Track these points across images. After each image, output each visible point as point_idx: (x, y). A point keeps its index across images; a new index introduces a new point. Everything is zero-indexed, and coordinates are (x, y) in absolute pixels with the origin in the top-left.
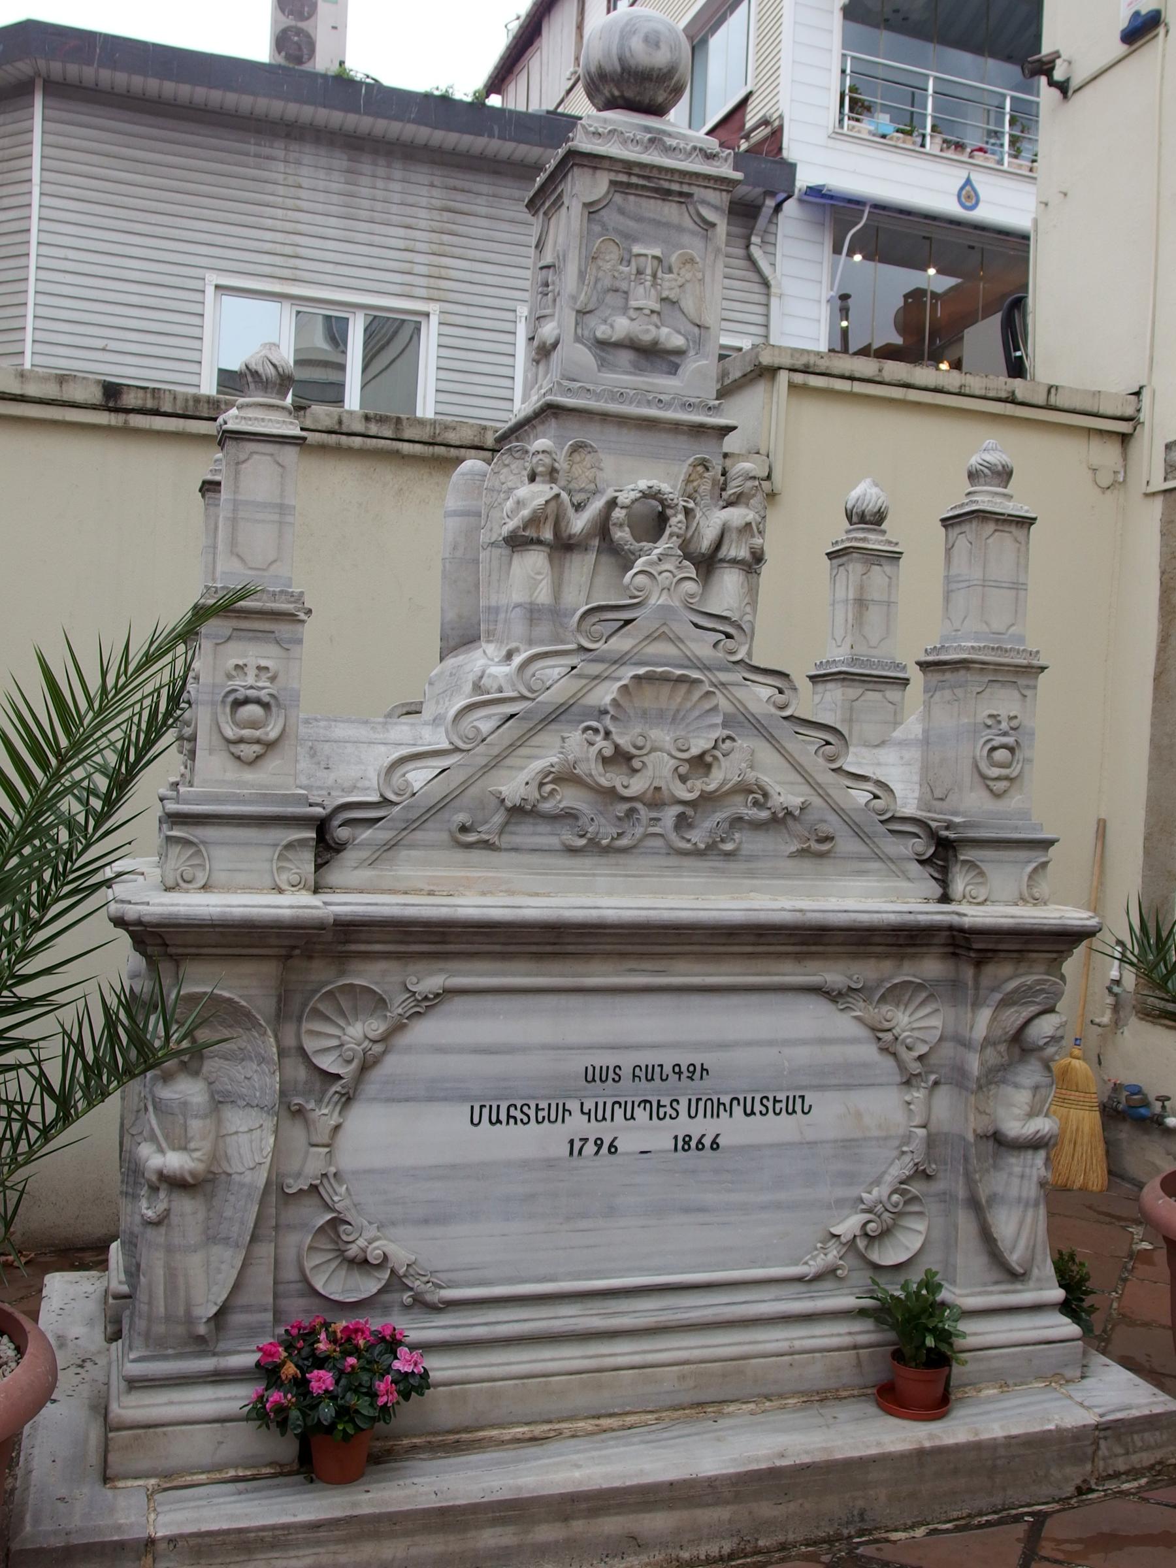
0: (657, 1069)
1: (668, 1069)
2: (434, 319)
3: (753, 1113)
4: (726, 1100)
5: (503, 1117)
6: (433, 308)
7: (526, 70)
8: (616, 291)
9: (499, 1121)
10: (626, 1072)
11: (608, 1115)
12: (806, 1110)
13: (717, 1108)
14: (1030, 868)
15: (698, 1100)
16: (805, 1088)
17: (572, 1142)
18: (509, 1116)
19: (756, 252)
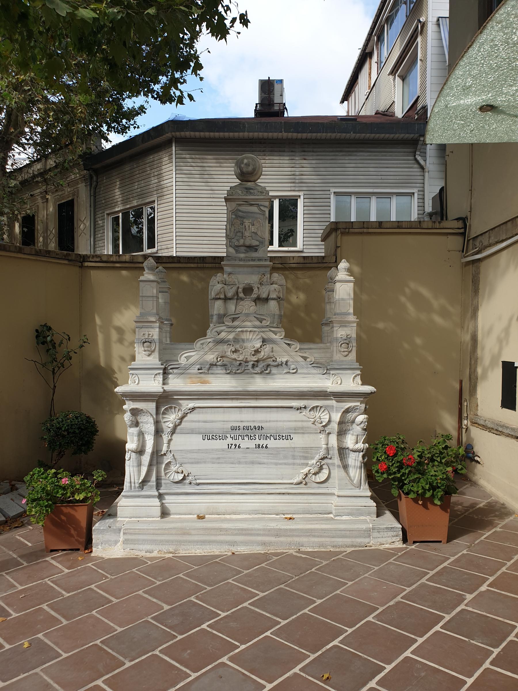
0: (250, 427)
1: (252, 427)
2: (302, 197)
3: (276, 439)
4: (269, 435)
5: (211, 438)
6: (301, 194)
7: (354, 92)
8: (240, 232)
9: (210, 439)
10: (241, 428)
11: (237, 438)
12: (291, 439)
13: (266, 438)
14: (354, 376)
15: (261, 435)
16: (290, 433)
17: (228, 445)
18: (212, 438)
19: (419, 158)
